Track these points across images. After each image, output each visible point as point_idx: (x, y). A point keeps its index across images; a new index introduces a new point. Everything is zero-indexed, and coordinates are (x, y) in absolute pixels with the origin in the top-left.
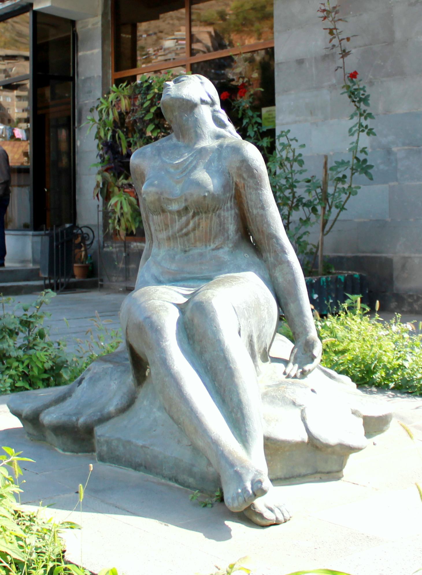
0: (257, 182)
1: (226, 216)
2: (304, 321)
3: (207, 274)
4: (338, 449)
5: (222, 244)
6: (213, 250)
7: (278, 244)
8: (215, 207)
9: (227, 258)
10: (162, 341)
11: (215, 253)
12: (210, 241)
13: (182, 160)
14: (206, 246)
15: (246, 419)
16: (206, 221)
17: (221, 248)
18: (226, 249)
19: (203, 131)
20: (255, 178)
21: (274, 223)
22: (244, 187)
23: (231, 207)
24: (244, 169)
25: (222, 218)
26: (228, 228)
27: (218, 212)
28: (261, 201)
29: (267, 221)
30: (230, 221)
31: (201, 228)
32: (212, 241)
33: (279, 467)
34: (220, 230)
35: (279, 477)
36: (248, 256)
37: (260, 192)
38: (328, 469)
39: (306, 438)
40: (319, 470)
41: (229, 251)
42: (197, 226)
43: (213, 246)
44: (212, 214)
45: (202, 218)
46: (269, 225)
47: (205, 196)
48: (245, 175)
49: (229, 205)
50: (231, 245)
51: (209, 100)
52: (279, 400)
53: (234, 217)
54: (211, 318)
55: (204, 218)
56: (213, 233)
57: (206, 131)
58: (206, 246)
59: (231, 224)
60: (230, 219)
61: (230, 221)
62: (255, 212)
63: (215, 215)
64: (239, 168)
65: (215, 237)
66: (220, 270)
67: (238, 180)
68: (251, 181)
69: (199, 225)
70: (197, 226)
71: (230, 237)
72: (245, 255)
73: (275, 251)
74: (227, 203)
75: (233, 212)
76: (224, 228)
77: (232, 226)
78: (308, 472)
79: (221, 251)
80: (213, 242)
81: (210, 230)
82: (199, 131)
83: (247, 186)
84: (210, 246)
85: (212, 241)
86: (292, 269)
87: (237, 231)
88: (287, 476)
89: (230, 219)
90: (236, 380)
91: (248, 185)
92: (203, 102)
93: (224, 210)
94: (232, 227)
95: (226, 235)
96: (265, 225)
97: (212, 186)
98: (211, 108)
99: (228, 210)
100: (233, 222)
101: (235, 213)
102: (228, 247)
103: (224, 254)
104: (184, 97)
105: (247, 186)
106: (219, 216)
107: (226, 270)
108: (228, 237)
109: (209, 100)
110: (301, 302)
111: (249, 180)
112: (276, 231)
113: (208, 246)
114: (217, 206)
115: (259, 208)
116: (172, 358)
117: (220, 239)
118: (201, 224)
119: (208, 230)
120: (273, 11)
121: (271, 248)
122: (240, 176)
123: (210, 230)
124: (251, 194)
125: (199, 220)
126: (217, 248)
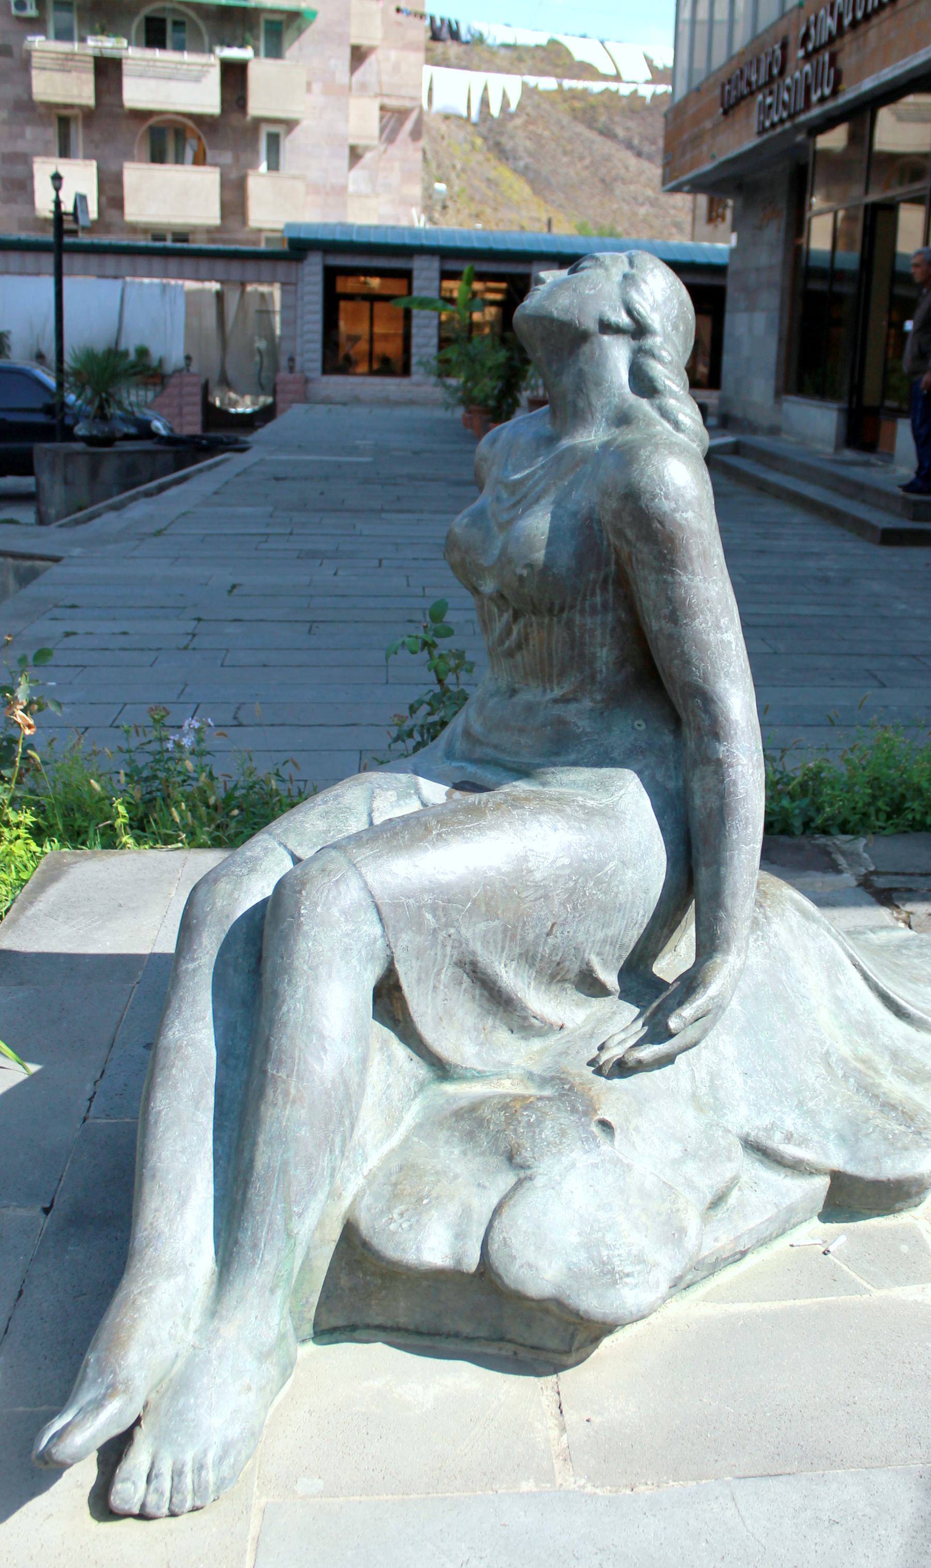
0: (660, 552)
1: (589, 626)
2: (717, 919)
3: (526, 758)
4: (553, 1307)
5: (575, 691)
6: (556, 701)
7: (707, 711)
8: (552, 604)
9: (584, 724)
10: (184, 958)
11: (559, 710)
12: (550, 681)
13: (532, 469)
14: (544, 691)
15: (246, 1211)
16: (538, 632)
17: (576, 700)
18: (587, 704)
19: (590, 404)
20: (656, 542)
21: (702, 660)
22: (631, 560)
23: (605, 606)
24: (627, 518)
25: (576, 630)
26: (594, 654)
27: (565, 615)
28: (669, 600)
29: (682, 651)
30: (599, 639)
31: (531, 647)
32: (555, 681)
33: (402, 1304)
34: (572, 658)
35: (400, 1325)
36: (643, 727)
37: (670, 579)
38: (534, 1341)
39: (472, 1262)
40: (508, 1337)
41: (592, 710)
42: (523, 641)
43: (557, 692)
44: (551, 620)
45: (531, 625)
46: (687, 663)
47: (521, 578)
48: (630, 534)
49: (598, 599)
50: (599, 697)
51: (623, 319)
52: (487, 1134)
53: (613, 629)
54: (282, 931)
55: (535, 625)
56: (555, 662)
57: (597, 403)
58: (544, 691)
59: (602, 646)
60: (598, 633)
61: (599, 639)
62: (655, 626)
63: (559, 622)
64: (617, 515)
65: (562, 673)
66: (557, 754)
67: (617, 543)
68: (646, 550)
69: (527, 639)
70: (523, 641)
71: (599, 677)
72: (632, 727)
73: (699, 729)
74: (593, 594)
75: (610, 617)
76: (582, 655)
77: (605, 650)
78: (481, 1334)
79: (573, 707)
80: (558, 683)
81: (550, 655)
82: (581, 404)
83: (637, 559)
84: (552, 690)
85: (555, 681)
86: (722, 781)
87: (621, 663)
88: (424, 1329)
89: (598, 633)
90: (263, 1107)
91: (639, 556)
92: (607, 327)
93: (582, 612)
94: (604, 655)
95: (588, 671)
96: (676, 662)
97: (543, 552)
98: (633, 343)
99: (594, 611)
100: (608, 640)
101: (619, 621)
102: (593, 700)
103: (579, 716)
104: (555, 314)
105: (637, 559)
106: (569, 625)
107: (573, 757)
108: (593, 678)
109: (623, 319)
110: (723, 870)
111: (639, 545)
112: (706, 680)
113: (548, 691)
114: (557, 602)
115: (665, 617)
116: (180, 1007)
117: (573, 679)
118: (530, 636)
119: (546, 655)
120: (76, 157)
121: (691, 718)
122: (620, 533)
123: (550, 655)
124: (645, 580)
125: (525, 626)
126: (564, 700)
